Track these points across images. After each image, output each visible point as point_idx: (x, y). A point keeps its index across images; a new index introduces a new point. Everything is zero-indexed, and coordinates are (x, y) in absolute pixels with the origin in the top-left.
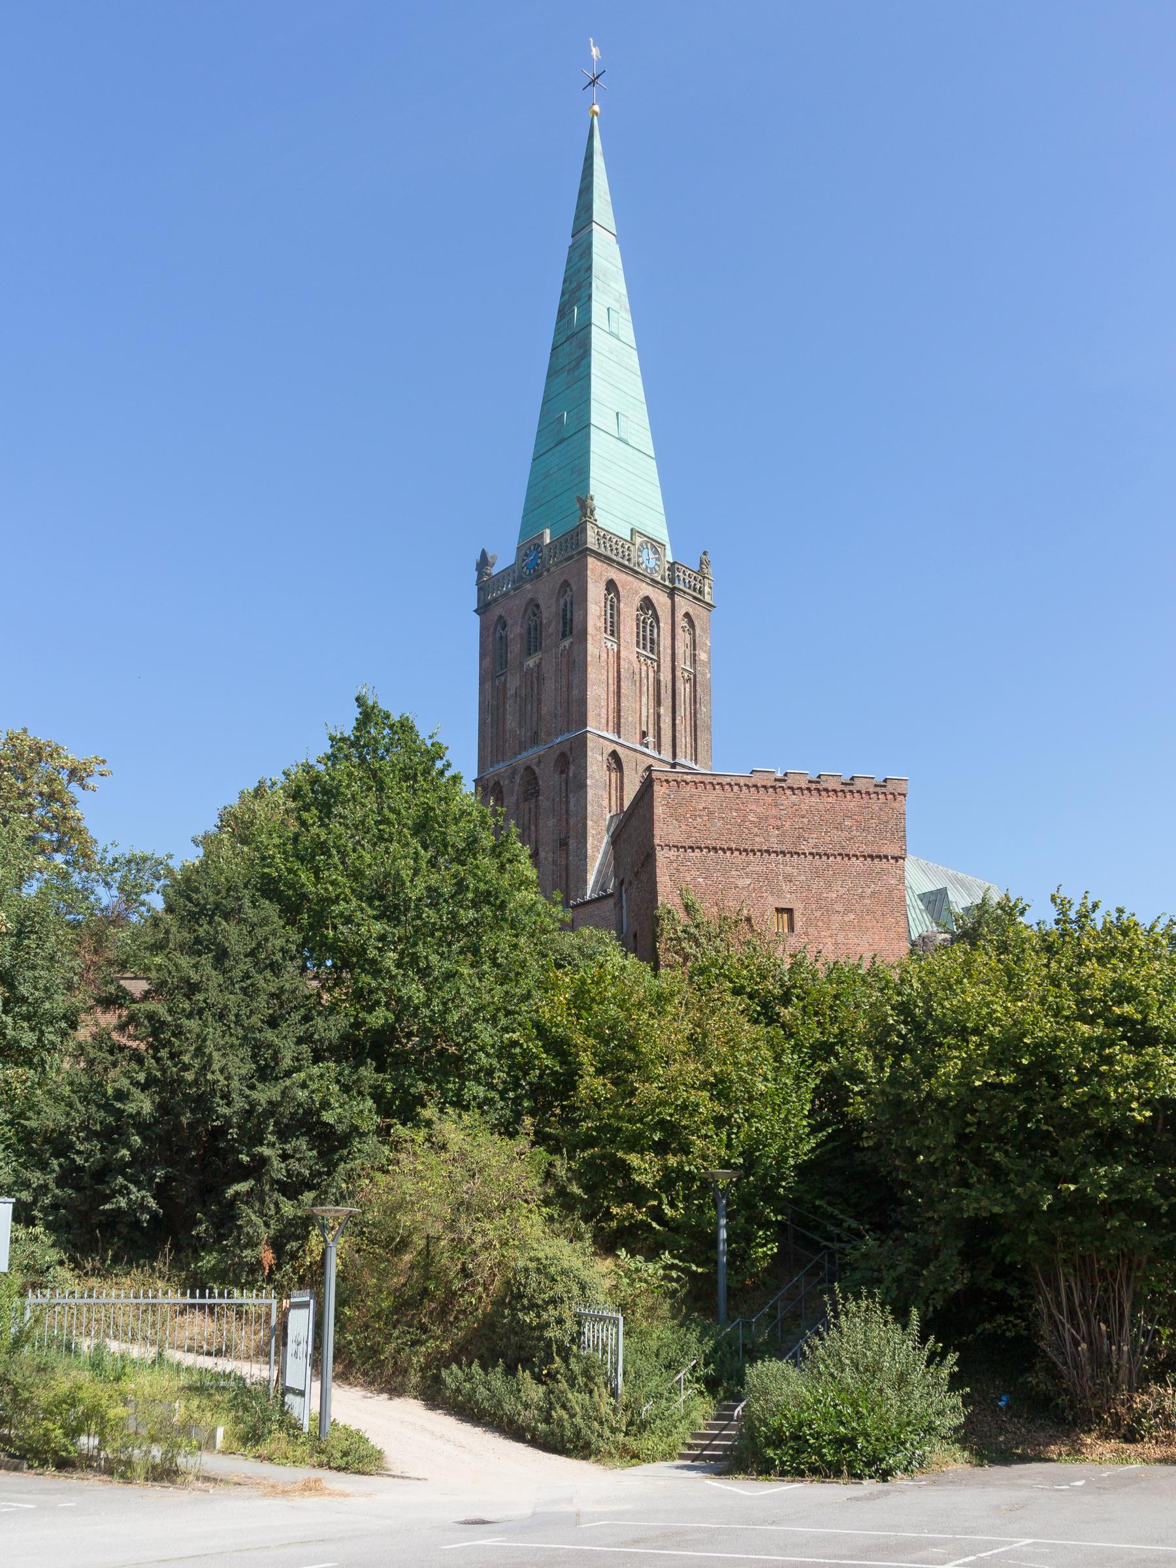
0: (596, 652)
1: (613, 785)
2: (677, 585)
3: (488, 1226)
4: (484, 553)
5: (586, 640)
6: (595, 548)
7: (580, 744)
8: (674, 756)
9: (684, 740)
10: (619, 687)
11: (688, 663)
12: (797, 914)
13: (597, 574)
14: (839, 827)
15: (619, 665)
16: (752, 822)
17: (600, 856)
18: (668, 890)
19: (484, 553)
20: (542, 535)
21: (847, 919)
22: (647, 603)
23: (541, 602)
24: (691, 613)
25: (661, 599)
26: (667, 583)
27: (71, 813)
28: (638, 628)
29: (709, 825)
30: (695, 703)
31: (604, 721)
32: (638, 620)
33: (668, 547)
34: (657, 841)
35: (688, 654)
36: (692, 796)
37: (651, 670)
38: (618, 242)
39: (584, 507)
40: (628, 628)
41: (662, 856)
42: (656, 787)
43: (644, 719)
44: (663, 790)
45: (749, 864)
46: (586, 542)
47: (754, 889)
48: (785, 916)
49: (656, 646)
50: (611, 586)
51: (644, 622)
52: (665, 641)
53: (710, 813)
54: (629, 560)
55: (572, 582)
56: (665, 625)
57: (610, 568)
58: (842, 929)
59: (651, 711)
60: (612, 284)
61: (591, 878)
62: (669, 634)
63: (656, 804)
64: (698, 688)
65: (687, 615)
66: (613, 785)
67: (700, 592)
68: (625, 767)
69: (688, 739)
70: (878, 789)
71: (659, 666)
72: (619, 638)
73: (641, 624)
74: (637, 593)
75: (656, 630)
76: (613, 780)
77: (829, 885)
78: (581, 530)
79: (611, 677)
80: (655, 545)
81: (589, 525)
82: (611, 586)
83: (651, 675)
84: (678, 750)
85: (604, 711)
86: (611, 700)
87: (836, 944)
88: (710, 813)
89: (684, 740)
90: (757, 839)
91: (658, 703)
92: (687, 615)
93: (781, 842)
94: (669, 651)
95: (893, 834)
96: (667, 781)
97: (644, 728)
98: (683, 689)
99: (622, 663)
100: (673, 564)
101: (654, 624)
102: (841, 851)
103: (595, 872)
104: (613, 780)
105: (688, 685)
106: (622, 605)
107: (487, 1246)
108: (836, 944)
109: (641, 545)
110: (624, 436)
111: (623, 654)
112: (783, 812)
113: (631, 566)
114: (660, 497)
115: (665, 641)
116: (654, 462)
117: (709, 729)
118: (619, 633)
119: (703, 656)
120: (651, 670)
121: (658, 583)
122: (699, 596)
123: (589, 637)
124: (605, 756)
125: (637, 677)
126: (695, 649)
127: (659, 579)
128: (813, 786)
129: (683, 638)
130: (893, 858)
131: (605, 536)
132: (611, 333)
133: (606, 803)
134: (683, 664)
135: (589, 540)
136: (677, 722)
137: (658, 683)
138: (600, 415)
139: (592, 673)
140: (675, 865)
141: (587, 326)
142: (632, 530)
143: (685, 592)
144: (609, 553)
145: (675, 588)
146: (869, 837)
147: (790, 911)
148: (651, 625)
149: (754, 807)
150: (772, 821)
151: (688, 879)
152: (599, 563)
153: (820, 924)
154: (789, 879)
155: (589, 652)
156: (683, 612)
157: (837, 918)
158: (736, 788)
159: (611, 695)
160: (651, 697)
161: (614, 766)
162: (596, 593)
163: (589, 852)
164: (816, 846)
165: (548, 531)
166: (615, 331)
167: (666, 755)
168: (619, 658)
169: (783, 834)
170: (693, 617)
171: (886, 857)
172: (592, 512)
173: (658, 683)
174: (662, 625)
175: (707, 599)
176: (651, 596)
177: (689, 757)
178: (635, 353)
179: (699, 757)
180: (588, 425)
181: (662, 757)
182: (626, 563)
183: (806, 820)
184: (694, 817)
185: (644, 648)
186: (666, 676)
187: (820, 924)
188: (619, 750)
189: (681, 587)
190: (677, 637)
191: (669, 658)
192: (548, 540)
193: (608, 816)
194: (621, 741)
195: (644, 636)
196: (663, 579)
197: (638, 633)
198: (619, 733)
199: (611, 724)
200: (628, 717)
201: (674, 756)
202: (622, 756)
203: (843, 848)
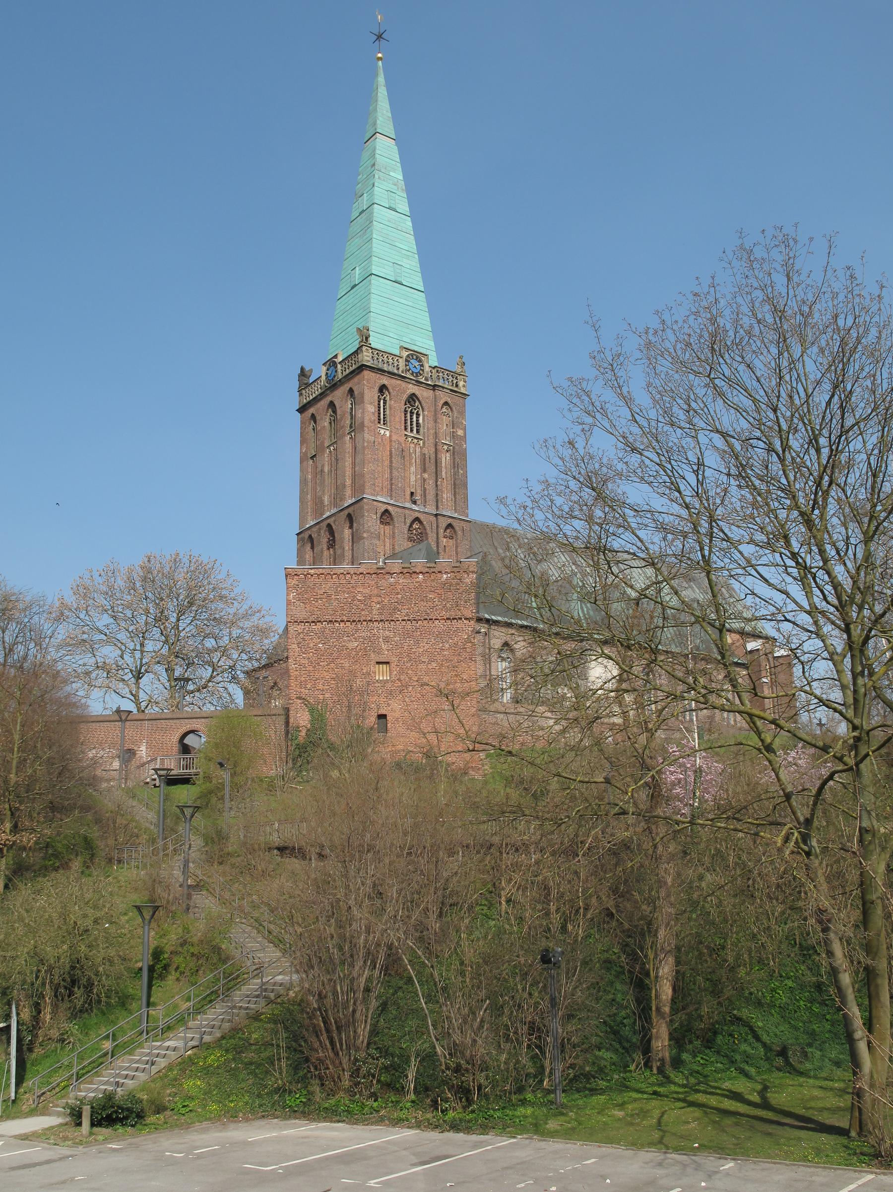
4: (302, 369)
8: (437, 508)
9: (446, 495)
14: (425, 599)
18: (296, 654)
19: (302, 369)
21: (430, 667)
23: (336, 403)
24: (450, 402)
26: (429, 383)
29: (327, 605)
32: (406, 411)
36: (314, 585)
38: (397, 144)
45: (357, 631)
54: (398, 369)
55: (355, 389)
57: (382, 377)
60: (392, 174)
68: (395, 519)
74: (405, 392)
77: (417, 642)
82: (383, 389)
83: (418, 450)
88: (330, 596)
89: (446, 495)
91: (424, 471)
93: (381, 614)
97: (413, 490)
98: (445, 459)
101: (421, 412)
105: (448, 455)
113: (400, 373)
114: (428, 319)
121: (422, 383)
124: (379, 515)
127: (423, 380)
128: (406, 571)
130: (466, 619)
140: (301, 635)
143: (443, 388)
144: (380, 366)
151: (311, 645)
152: (373, 374)
153: (410, 672)
156: (442, 402)
157: (422, 666)
164: (407, 615)
169: (383, 608)
175: (463, 390)
176: (417, 393)
182: (396, 371)
183: (400, 596)
184: (316, 600)
187: (410, 672)
188: (390, 508)
196: (427, 379)
197: (406, 420)
198: (391, 496)
201: (437, 508)
202: (393, 513)
203: (428, 614)
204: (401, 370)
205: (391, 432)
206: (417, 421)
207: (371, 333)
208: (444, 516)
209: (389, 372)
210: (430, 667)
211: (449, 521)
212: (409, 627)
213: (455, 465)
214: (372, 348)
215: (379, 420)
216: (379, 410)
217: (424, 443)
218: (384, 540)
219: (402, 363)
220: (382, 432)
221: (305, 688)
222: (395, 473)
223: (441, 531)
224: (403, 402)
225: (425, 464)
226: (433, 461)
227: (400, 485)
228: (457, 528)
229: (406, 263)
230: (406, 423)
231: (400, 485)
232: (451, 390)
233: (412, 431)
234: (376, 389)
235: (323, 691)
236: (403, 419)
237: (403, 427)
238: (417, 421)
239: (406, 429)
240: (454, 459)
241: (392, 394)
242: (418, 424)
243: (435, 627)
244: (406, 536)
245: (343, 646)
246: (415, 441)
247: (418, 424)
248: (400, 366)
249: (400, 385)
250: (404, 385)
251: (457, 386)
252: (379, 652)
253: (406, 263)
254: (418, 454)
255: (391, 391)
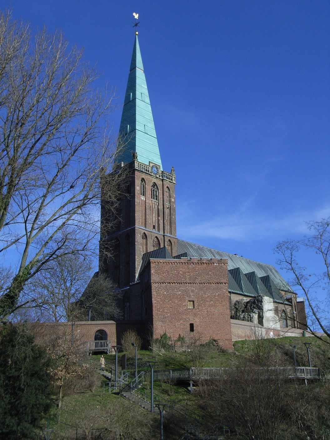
0: (138, 201)
1: (144, 243)
2: (164, 178)
3: (6, 162)
5: (135, 197)
6: (137, 169)
7: (133, 231)
8: (164, 233)
9: (167, 227)
10: (146, 212)
11: (168, 202)
12: (195, 302)
13: (138, 177)
14: (208, 274)
15: (145, 205)
16: (181, 274)
17: (140, 267)
18: (155, 296)
20: (121, 164)
22: (155, 185)
24: (169, 187)
25: (159, 183)
26: (161, 178)
27: (33, 340)
28: (152, 192)
30: (171, 215)
31: (141, 223)
32: (152, 190)
33: (161, 166)
34: (152, 281)
35: (168, 199)
37: (156, 205)
39: (134, 156)
40: (149, 193)
41: (154, 286)
42: (152, 265)
43: (154, 221)
44: (154, 265)
46: (135, 167)
47: (182, 295)
48: (192, 302)
49: (158, 198)
50: (143, 180)
51: (154, 190)
52: (161, 196)
53: (168, 272)
54: (148, 171)
56: (160, 191)
58: (209, 306)
59: (156, 218)
61: (137, 275)
62: (162, 194)
63: (151, 269)
64: (171, 210)
65: (167, 187)
66: (144, 243)
67: (171, 180)
69: (168, 227)
70: (219, 262)
71: (158, 204)
72: (145, 196)
73: (153, 191)
75: (157, 193)
76: (144, 242)
78: (133, 163)
79: (143, 208)
80: (156, 167)
81: (135, 162)
82: (143, 180)
83: (156, 207)
84: (165, 231)
85: (141, 220)
86: (143, 216)
87: (207, 311)
89: (167, 227)
90: (183, 279)
91: (159, 216)
92: (167, 187)
94: (162, 199)
95: (224, 276)
96: (155, 262)
97: (154, 224)
98: (167, 211)
99: (147, 204)
100: (163, 172)
102: (208, 282)
103: (138, 273)
104: (144, 242)
105: (168, 210)
106: (146, 186)
107: (29, 364)
108: (207, 311)
109: (152, 166)
110: (146, 132)
111: (147, 201)
112: (190, 271)
114: (158, 150)
115: (161, 196)
116: (156, 139)
117: (175, 223)
118: (145, 195)
119: (173, 200)
120: (156, 205)
121: (158, 178)
122: (171, 181)
123: (136, 197)
125: (152, 208)
126: (170, 198)
128: (199, 262)
129: (166, 194)
131: (140, 164)
132: (142, 101)
133: (142, 250)
134: (167, 204)
135: (136, 166)
136: (165, 222)
137: (158, 209)
138: (139, 126)
139: (137, 208)
140: (157, 288)
141: (134, 98)
142: (149, 162)
145: (163, 179)
146: (217, 277)
147: (193, 301)
148: (156, 191)
149: (181, 269)
150: (187, 274)
153: (202, 305)
154: (193, 291)
155: (136, 201)
156: (166, 186)
158: (176, 263)
159: (143, 214)
160: (156, 214)
161: (145, 237)
162: (138, 182)
163: (136, 266)
164: (200, 281)
165: (123, 163)
166: (144, 100)
167: (161, 232)
168: (145, 202)
170: (169, 188)
171: (222, 283)
172: (136, 158)
173: (158, 209)
174: (159, 191)
175: (174, 182)
177: (169, 233)
178: (150, 106)
179: (172, 233)
180: (135, 129)
181: (160, 233)
182: (148, 172)
183: (197, 273)
185: (154, 199)
186: (161, 207)
187: (202, 305)
188: (146, 232)
189: (165, 179)
190: (164, 195)
191: (162, 201)
192: (123, 165)
193: (142, 254)
194: (147, 229)
195: (154, 195)
196: (160, 176)
197: (152, 194)
199: (143, 224)
200: (149, 221)
201: (164, 233)
202: (147, 234)
203: (209, 281)
204: (149, 172)
205: (145, 198)
206: (156, 194)
207: (138, 156)
208: (167, 236)
209: (145, 173)
210: (210, 303)
211: (169, 238)
212: (201, 286)
213: (170, 214)
214: (139, 162)
215: (141, 193)
216: (141, 189)
217: (158, 204)
218: (143, 246)
219: (150, 169)
220: (142, 198)
221: (160, 311)
222: (147, 217)
223: (166, 243)
224: (150, 186)
225: (159, 213)
226: (162, 212)
227: (149, 222)
228: (172, 242)
229: (149, 125)
230: (152, 195)
231: (149, 222)
232: (170, 182)
233: (154, 199)
234: (140, 180)
235: (167, 312)
236: (151, 193)
237: (151, 197)
238: (156, 194)
239: (152, 198)
240: (170, 211)
241: (146, 182)
242: (156, 196)
243: (212, 286)
244: (152, 244)
245: (175, 293)
246: (155, 203)
247: (156, 196)
248: (149, 170)
249: (149, 178)
250: (151, 178)
251: (171, 180)
252: (190, 296)
253: (149, 125)
254: (156, 209)
255: (146, 181)
